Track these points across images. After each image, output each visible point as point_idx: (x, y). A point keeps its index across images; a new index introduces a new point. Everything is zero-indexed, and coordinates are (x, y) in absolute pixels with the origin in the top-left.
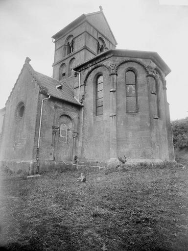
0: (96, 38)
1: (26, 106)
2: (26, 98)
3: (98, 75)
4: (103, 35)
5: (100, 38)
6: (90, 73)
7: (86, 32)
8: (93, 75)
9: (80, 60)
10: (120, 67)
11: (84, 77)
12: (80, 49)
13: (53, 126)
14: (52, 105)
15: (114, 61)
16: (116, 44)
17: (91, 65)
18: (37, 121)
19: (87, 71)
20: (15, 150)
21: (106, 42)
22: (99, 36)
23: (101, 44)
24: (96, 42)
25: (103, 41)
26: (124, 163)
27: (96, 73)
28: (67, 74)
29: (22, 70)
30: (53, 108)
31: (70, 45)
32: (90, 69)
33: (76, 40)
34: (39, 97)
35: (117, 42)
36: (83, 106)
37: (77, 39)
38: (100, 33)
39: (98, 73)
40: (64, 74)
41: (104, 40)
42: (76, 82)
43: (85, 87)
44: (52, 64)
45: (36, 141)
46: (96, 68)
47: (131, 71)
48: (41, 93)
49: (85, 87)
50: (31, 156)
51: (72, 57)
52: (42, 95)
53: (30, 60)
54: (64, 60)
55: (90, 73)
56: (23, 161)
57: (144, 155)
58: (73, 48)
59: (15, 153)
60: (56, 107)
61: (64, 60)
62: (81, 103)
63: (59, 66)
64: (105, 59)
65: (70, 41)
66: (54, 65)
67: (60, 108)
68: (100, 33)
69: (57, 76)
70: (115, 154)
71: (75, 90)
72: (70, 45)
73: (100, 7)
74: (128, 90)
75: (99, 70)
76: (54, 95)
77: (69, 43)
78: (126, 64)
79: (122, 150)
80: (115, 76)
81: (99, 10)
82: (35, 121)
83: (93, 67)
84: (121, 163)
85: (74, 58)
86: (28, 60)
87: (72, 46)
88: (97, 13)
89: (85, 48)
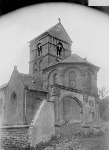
0: (56, 45)
1: (17, 95)
2: (17, 90)
3: (55, 75)
4: (61, 40)
5: (59, 43)
6: (51, 73)
7: (49, 43)
8: (52, 74)
9: (44, 66)
10: (65, 73)
11: (48, 75)
12: (45, 54)
13: (31, 105)
14: (31, 94)
15: (62, 68)
16: (72, 43)
17: (51, 68)
18: (24, 103)
19: (49, 72)
20: (13, 117)
21: (64, 44)
22: (58, 42)
23: (60, 46)
24: (56, 47)
25: (61, 45)
26: (67, 122)
27: (54, 73)
28: (38, 70)
29: (13, 73)
30: (31, 95)
31: (40, 50)
32: (51, 70)
33: (43, 47)
34: (24, 92)
35: (73, 41)
36: (48, 92)
37: (43, 46)
38: (58, 40)
39: (55, 74)
40: (36, 70)
41: (62, 43)
42: (43, 77)
43: (48, 81)
44: (29, 62)
45: (24, 113)
46: (54, 70)
47: (71, 72)
48: (24, 88)
49: (48, 81)
50: (22, 120)
51: (41, 59)
52: (25, 89)
53: (17, 67)
54: (36, 60)
55: (51, 73)
56: (18, 123)
57: (24, 124)
58: (41, 52)
59: (13, 119)
60: (33, 95)
61: (36, 60)
62: (47, 90)
63: (33, 63)
64: (58, 66)
65: (39, 46)
66: (30, 63)
67: (35, 95)
68: (58, 40)
69: (32, 72)
70: (62, 118)
71: (43, 82)
72: (40, 50)
73: (59, 19)
74: (71, 83)
75: (55, 72)
76: (31, 89)
77: (38, 48)
78: (70, 69)
79: (67, 116)
80: (63, 77)
81: (58, 22)
82: (23, 103)
83: (52, 70)
84: (66, 123)
85: (42, 60)
86: (16, 67)
87: (41, 50)
88: (58, 24)
89: (49, 54)
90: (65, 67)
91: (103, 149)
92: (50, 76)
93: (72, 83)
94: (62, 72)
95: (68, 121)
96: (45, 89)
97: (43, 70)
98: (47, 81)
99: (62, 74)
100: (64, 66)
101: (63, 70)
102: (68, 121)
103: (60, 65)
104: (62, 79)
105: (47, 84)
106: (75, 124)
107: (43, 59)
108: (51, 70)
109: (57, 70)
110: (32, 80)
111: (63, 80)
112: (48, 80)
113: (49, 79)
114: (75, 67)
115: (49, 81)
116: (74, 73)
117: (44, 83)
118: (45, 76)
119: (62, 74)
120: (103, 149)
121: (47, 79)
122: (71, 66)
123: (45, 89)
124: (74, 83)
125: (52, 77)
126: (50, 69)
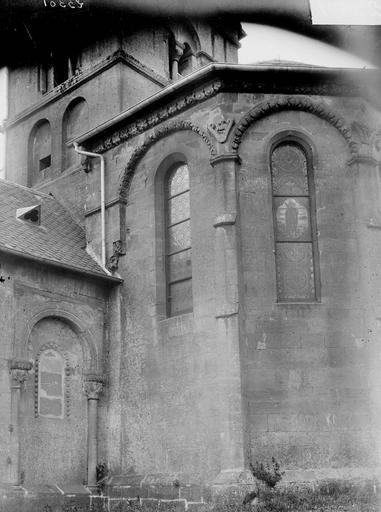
13: (10, 361)
15: (227, 109)
17: (142, 125)
19: (127, 152)
26: (271, 484)
27: (161, 157)
28: (56, 160)
32: (141, 140)
36: (119, 283)
40: (46, 162)
43: (123, 212)
46: (160, 136)
49: (123, 212)
51: (72, 97)
55: (139, 156)
62: (113, 269)
64: (196, 102)
67: (33, 292)
70: (237, 455)
71: (88, 222)
74: (282, 215)
75: (170, 145)
83: (152, 132)
85: (80, 100)
90: (247, 104)
91: (1, 280)
92: (137, 176)
93: (292, 211)
94: (223, 137)
95: (278, 477)
96: (102, 263)
97: (89, 143)
98: (115, 210)
99: (227, 150)
100: (240, 96)
101: (230, 121)
102: (272, 472)
103: (210, 90)
104: (225, 180)
105: (115, 228)
106: (323, 491)
107: (82, 92)
108: (141, 140)
109: (190, 128)
110: (19, 205)
111: (231, 186)
112: (123, 202)
113: (130, 198)
114: (307, 109)
115: (129, 209)
116: (296, 150)
117: (93, 224)
118: (101, 187)
119: (227, 150)
120: (1, 280)
121: (115, 198)
122: (280, 99)
123: (102, 263)
124: (302, 212)
125: (150, 184)
126: (134, 130)
